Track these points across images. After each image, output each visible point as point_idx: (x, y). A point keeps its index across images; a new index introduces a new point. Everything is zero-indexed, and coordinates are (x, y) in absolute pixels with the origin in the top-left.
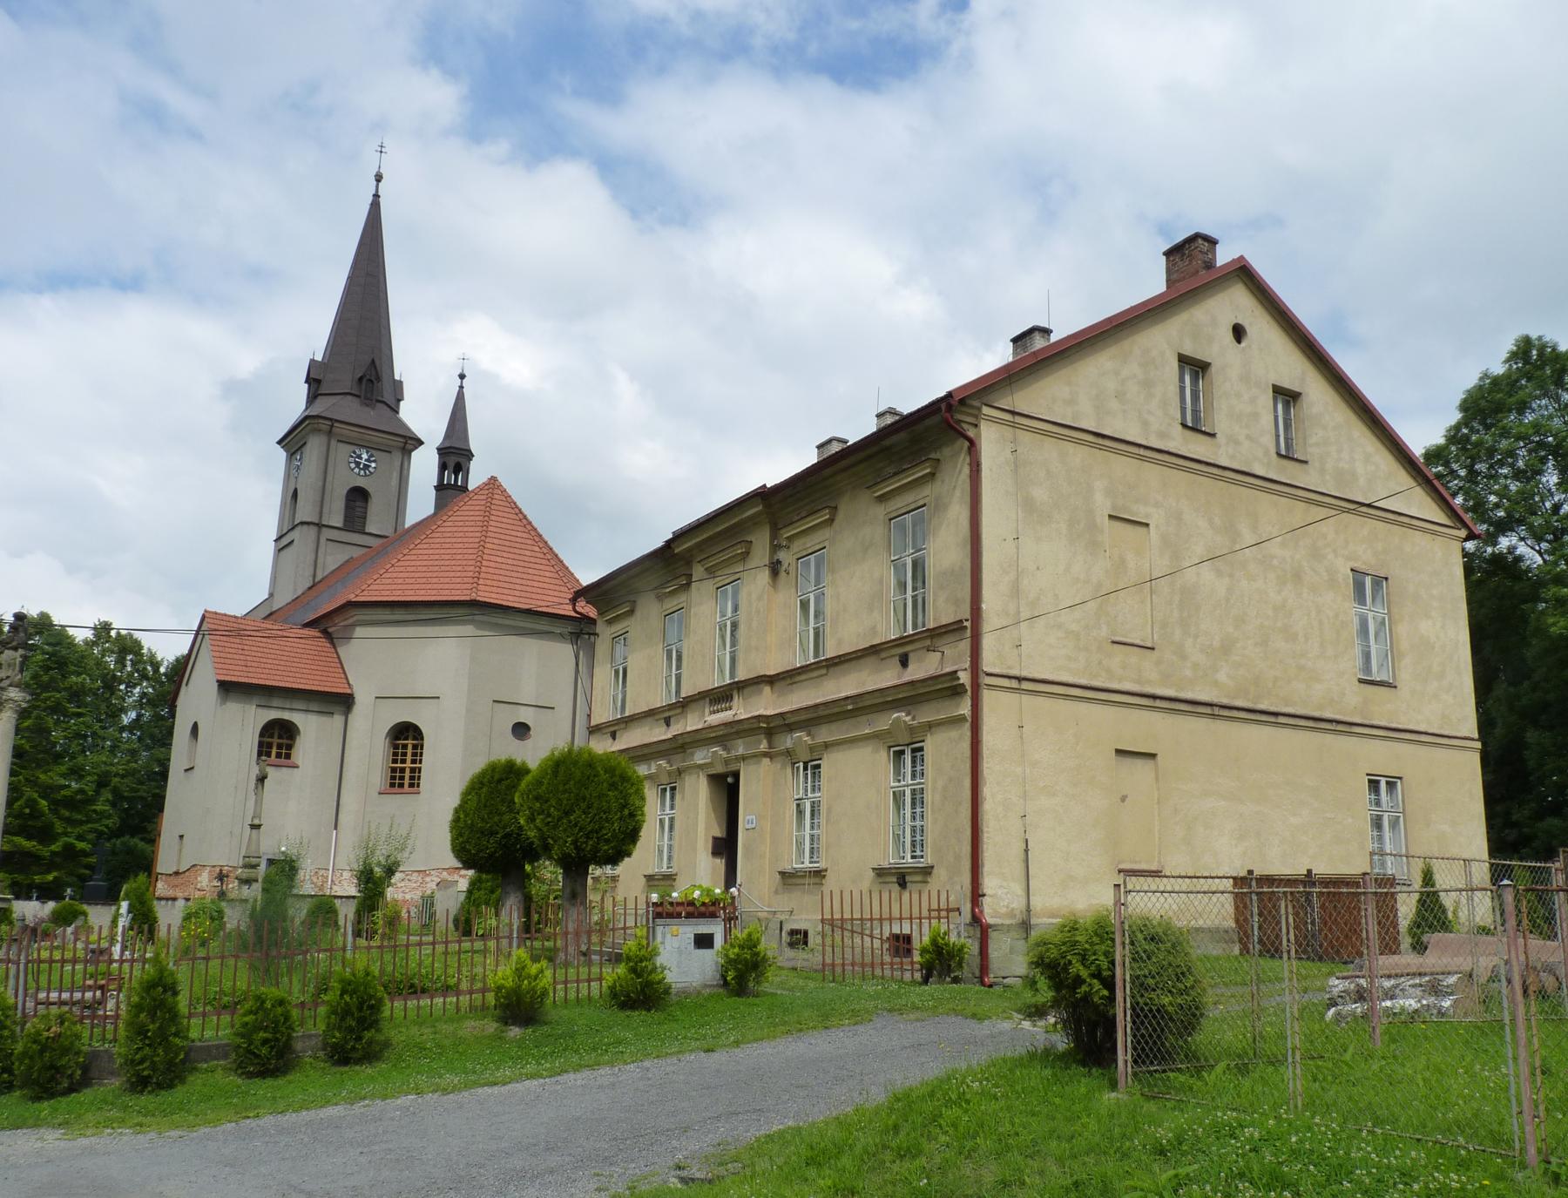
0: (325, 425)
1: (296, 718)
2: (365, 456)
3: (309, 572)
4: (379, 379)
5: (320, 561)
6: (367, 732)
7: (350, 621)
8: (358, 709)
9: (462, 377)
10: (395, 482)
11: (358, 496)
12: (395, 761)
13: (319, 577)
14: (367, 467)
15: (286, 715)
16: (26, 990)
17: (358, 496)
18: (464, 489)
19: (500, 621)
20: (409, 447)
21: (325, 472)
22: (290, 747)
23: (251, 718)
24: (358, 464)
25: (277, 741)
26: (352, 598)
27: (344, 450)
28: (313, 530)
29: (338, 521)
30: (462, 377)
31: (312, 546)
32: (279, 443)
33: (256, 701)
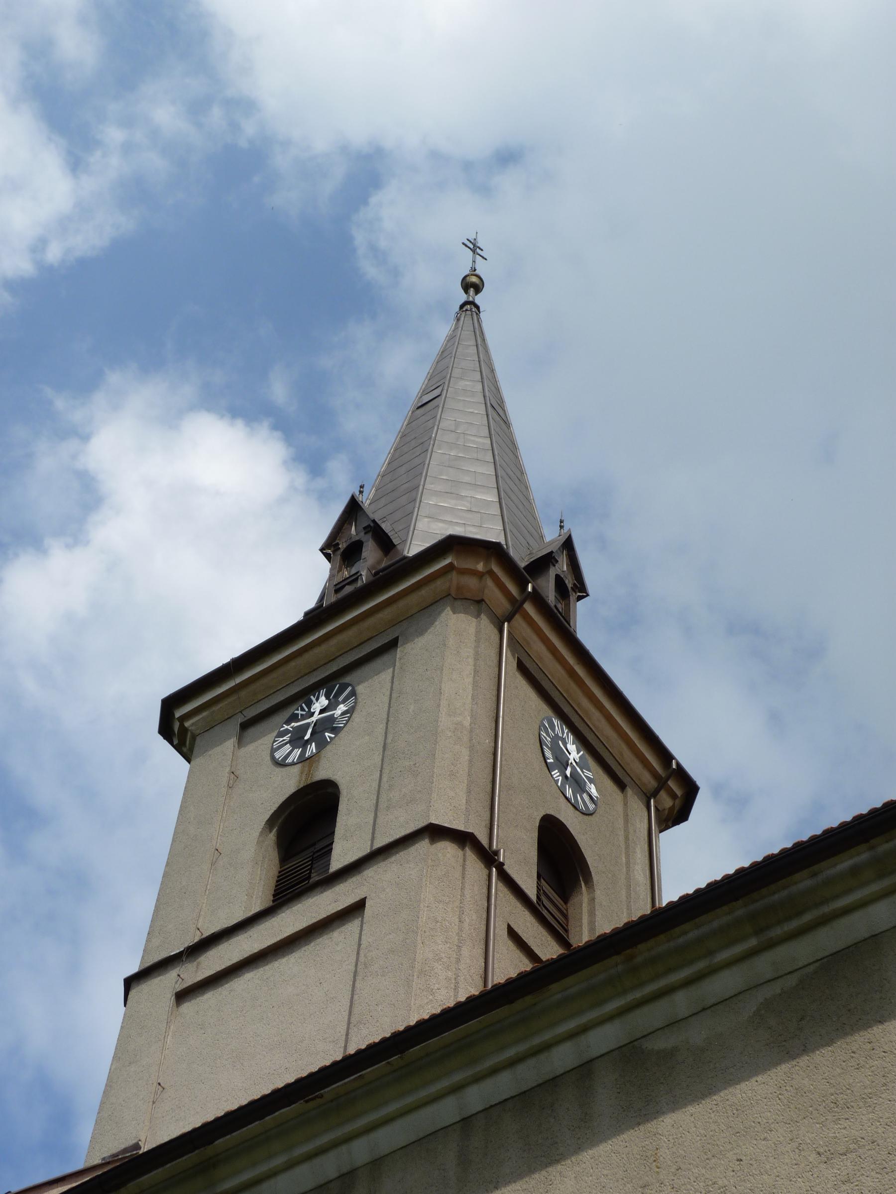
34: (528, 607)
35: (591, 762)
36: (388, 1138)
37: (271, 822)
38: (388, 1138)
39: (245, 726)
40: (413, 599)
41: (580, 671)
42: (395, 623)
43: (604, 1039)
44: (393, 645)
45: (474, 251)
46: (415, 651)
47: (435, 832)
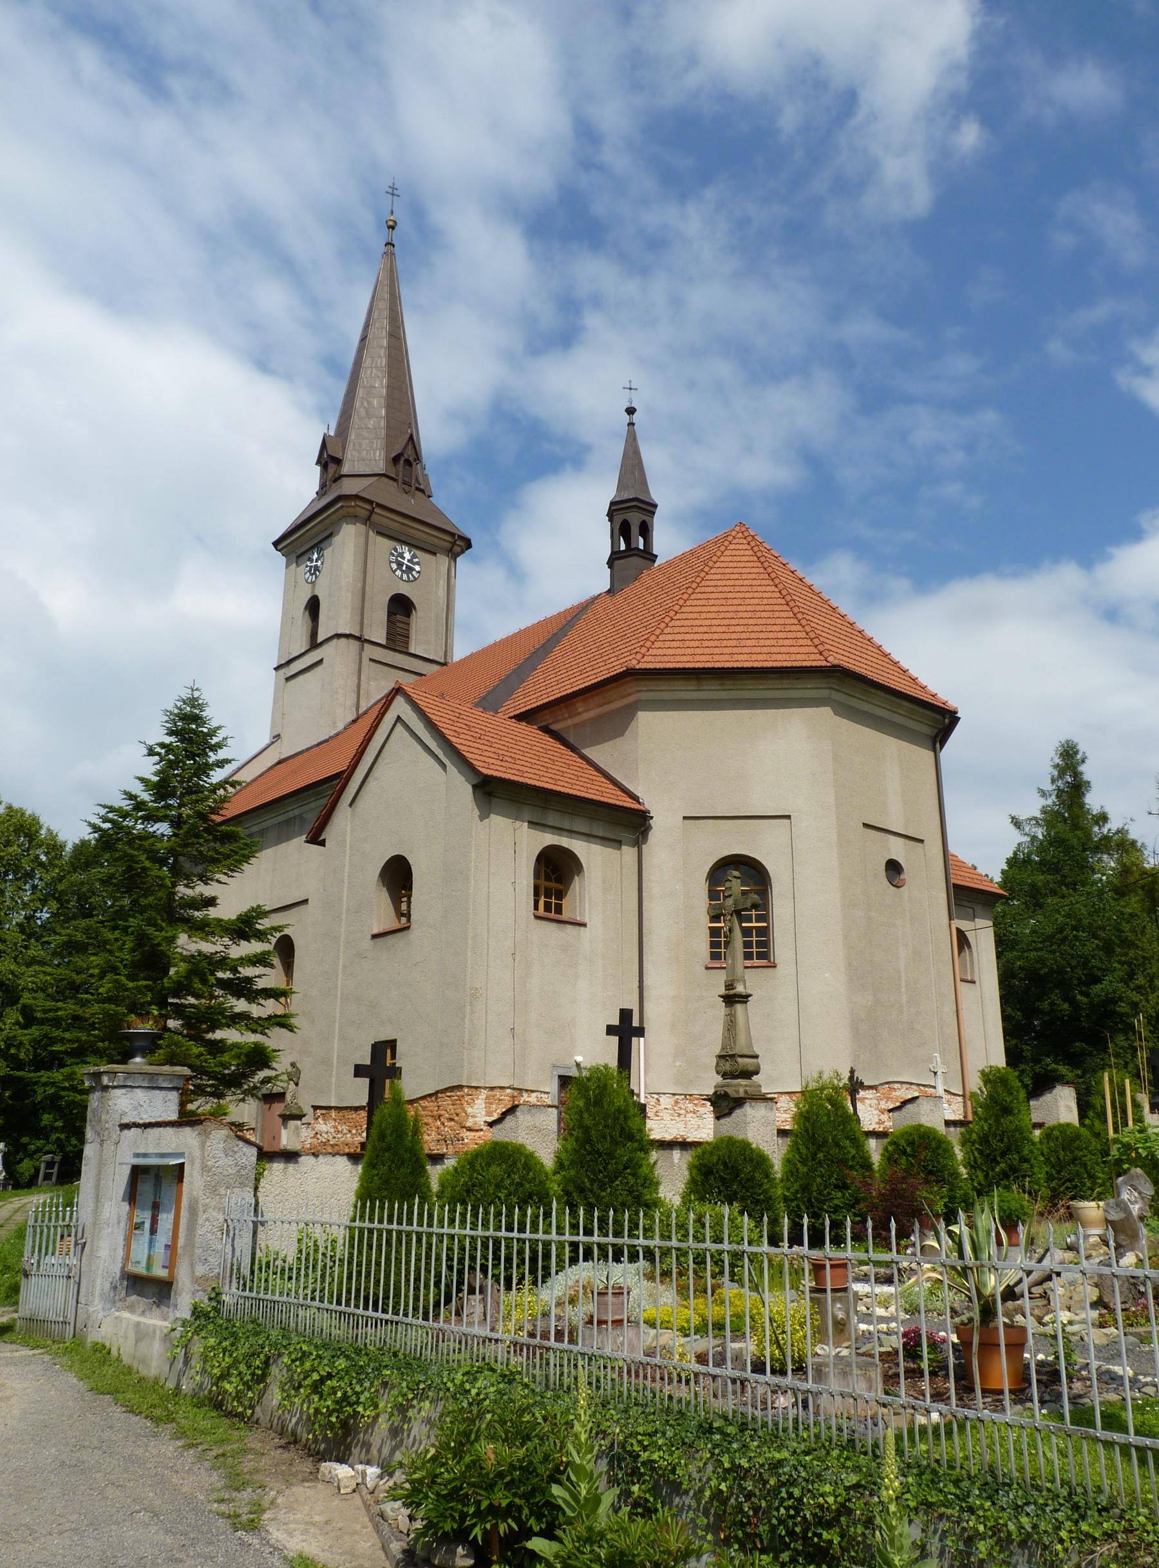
0: (362, 510)
1: (577, 846)
2: (407, 556)
3: (351, 700)
4: (418, 458)
5: (363, 686)
6: (675, 866)
7: (630, 699)
8: (654, 836)
9: (631, 411)
10: (442, 593)
11: (401, 606)
12: (715, 918)
13: (361, 711)
14: (410, 569)
15: (565, 842)
16: (47, 1248)
17: (401, 606)
18: (649, 556)
19: (867, 707)
20: (457, 549)
21: (365, 572)
22: (560, 895)
23: (517, 843)
24: (400, 565)
25: (555, 874)
26: (634, 664)
27: (385, 544)
28: (354, 644)
29: (380, 636)
30: (631, 411)
31: (353, 667)
32: (276, 544)
33: (527, 813)
34: (377, 510)
35: (418, 553)
36: (268, 824)
37: (306, 608)
38: (268, 824)
39: (298, 557)
40: (334, 517)
41: (405, 521)
42: (332, 524)
43: (297, 812)
44: (330, 535)
45: (393, 194)
46: (337, 540)
47: (338, 636)
